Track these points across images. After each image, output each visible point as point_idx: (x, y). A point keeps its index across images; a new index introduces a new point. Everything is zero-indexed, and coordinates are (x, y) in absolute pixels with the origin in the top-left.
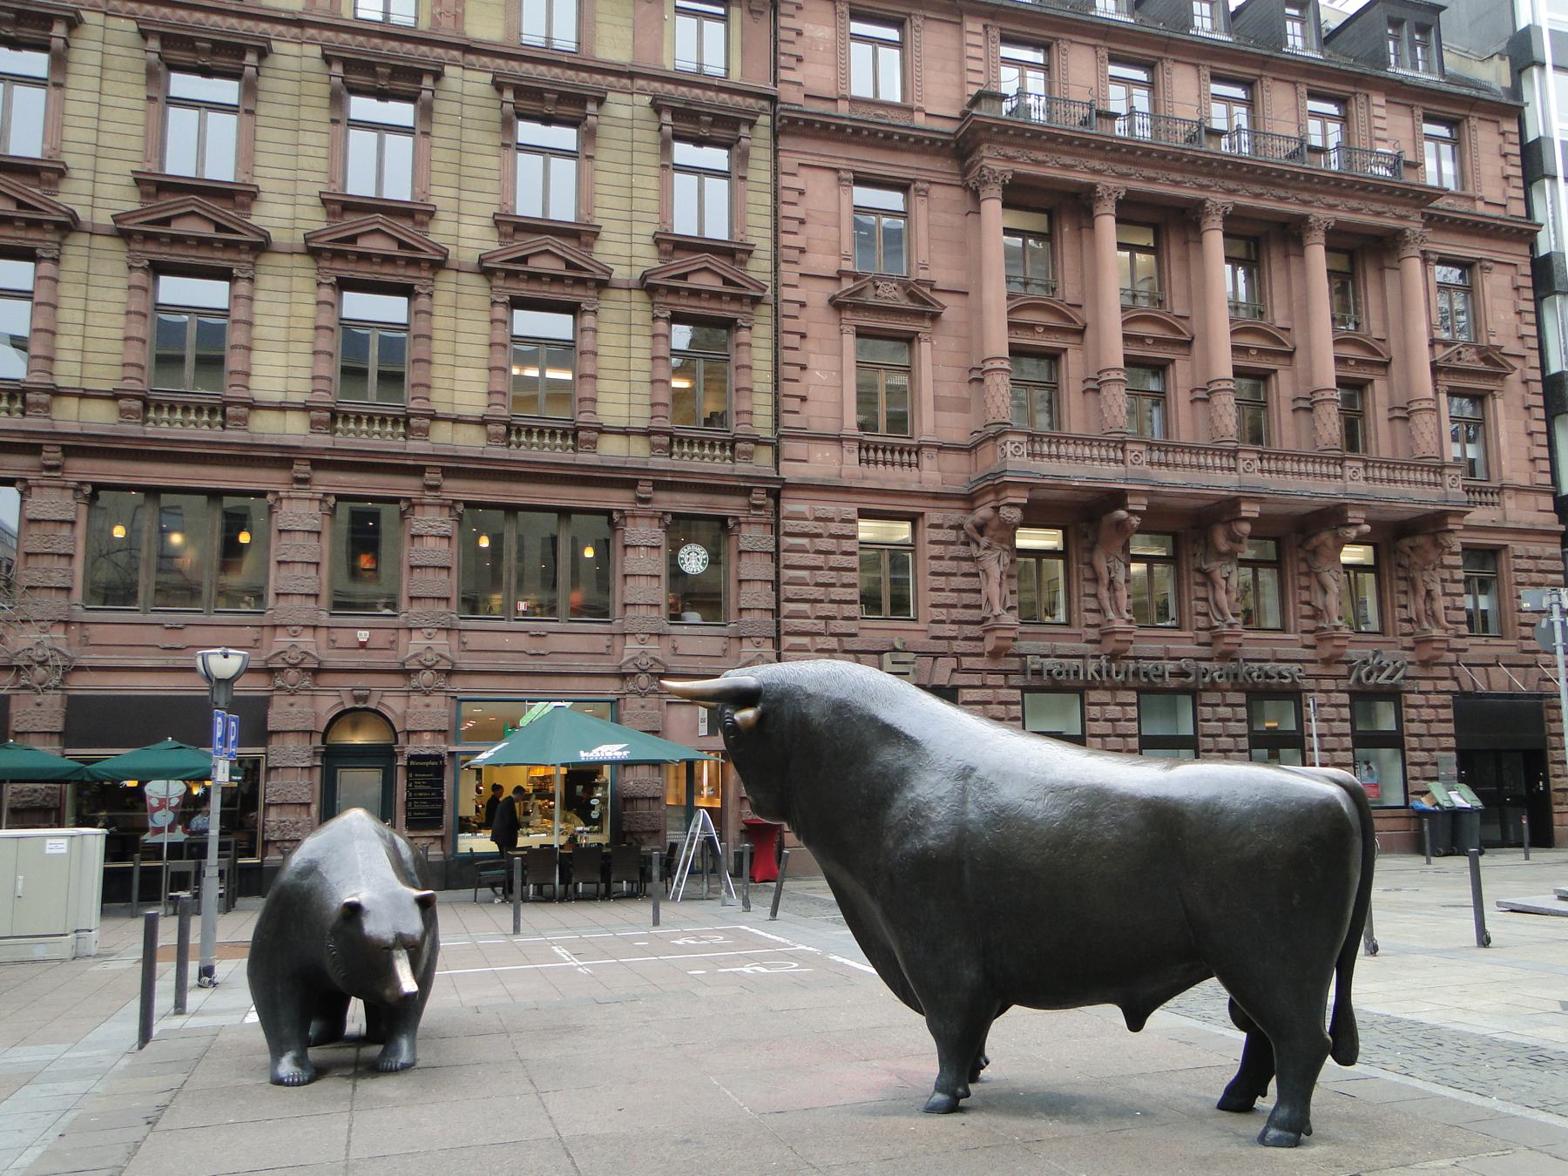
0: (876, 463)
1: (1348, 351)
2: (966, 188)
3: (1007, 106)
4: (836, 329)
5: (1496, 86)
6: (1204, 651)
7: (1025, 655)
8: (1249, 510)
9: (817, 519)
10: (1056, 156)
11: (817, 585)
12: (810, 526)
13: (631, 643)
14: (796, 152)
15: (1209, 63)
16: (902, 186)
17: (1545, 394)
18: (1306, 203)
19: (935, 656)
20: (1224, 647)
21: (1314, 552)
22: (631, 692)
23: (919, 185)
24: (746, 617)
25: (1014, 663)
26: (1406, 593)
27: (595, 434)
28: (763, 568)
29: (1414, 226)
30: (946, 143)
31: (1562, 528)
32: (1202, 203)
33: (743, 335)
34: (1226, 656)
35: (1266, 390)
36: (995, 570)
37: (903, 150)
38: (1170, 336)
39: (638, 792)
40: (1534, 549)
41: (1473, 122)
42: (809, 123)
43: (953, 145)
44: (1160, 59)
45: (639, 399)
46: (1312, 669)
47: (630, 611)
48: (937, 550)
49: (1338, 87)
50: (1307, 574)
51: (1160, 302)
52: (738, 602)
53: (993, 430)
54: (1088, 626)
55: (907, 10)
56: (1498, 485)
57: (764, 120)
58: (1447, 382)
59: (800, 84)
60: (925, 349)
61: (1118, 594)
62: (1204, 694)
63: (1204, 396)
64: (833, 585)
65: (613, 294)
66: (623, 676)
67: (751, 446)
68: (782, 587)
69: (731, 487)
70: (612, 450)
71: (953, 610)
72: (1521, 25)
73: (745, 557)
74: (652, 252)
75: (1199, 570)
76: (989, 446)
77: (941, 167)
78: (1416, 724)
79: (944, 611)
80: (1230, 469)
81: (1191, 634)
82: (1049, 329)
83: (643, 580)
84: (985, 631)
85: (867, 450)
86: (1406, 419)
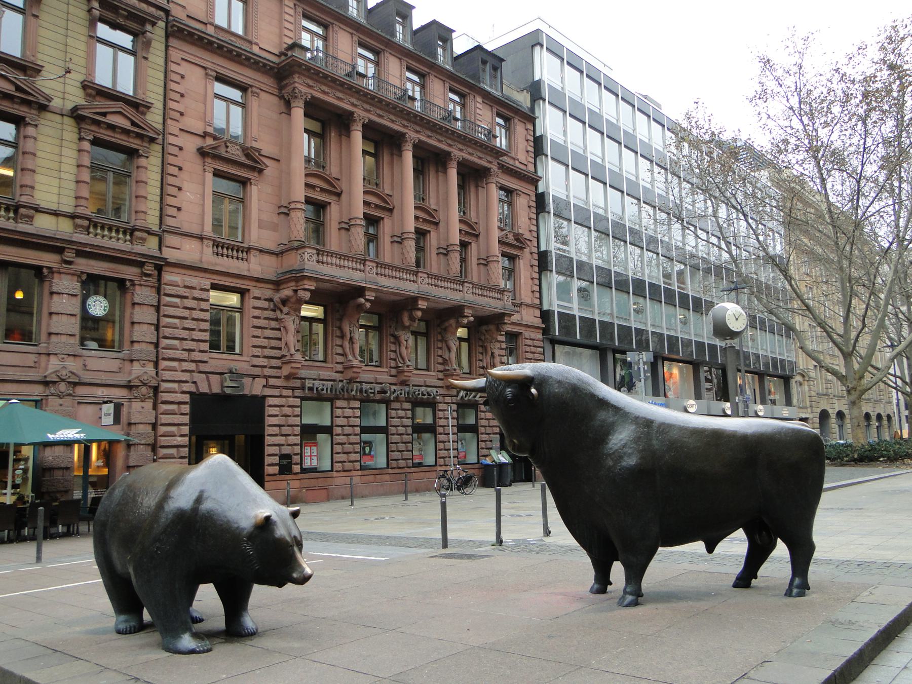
0: (222, 255)
1: (313, 181)
2: (281, 97)
3: (309, 55)
4: (201, 168)
5: (524, 105)
6: (393, 380)
7: (304, 379)
8: (422, 304)
9: (186, 287)
10: (334, 91)
11: (184, 329)
12: (181, 291)
13: (53, 360)
14: (180, 50)
15: (358, 35)
16: (243, 88)
17: (539, 260)
18: (450, 145)
19: (254, 377)
20: (404, 378)
21: (445, 330)
22: (53, 395)
23: (254, 89)
24: (136, 346)
25: (298, 383)
26: (482, 353)
27: (33, 212)
28: (149, 315)
29: (494, 168)
30: (272, 68)
31: (543, 326)
32: (404, 135)
33: (142, 161)
34: (404, 383)
35: (424, 239)
36: (292, 328)
37: (247, 66)
38: (383, 204)
39: (55, 464)
40: (533, 336)
41: (432, 77)
42: (191, 34)
43: (276, 70)
44: (383, 50)
45: (67, 192)
46: (441, 391)
47: (54, 339)
48: (257, 313)
49: (372, 42)
50: (441, 341)
51: (423, 200)
52: (131, 336)
53: (296, 244)
54: (337, 363)
55: (332, 21)
56: (247, 246)
57: (161, 24)
58: (212, 164)
59: (184, 7)
60: (254, 191)
61: (354, 345)
62: (392, 403)
63: (398, 240)
64: (193, 330)
65: (49, 115)
66: (46, 383)
67: (145, 235)
68: (161, 329)
69: (133, 260)
70: (44, 224)
71: (264, 350)
72: (537, 78)
73: (137, 308)
74: (80, 93)
75: (393, 335)
76: (293, 253)
77: (265, 81)
78: (442, 420)
79: (260, 350)
80: (414, 281)
81: (248, 359)
82: (323, 190)
83: (65, 318)
84: (283, 363)
85: (217, 247)
86: (486, 265)
